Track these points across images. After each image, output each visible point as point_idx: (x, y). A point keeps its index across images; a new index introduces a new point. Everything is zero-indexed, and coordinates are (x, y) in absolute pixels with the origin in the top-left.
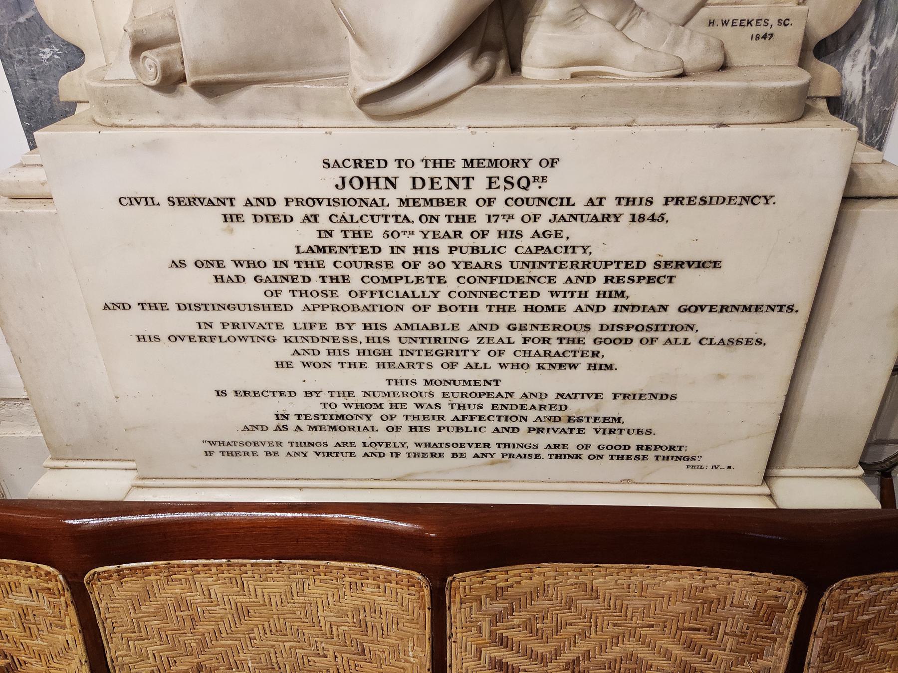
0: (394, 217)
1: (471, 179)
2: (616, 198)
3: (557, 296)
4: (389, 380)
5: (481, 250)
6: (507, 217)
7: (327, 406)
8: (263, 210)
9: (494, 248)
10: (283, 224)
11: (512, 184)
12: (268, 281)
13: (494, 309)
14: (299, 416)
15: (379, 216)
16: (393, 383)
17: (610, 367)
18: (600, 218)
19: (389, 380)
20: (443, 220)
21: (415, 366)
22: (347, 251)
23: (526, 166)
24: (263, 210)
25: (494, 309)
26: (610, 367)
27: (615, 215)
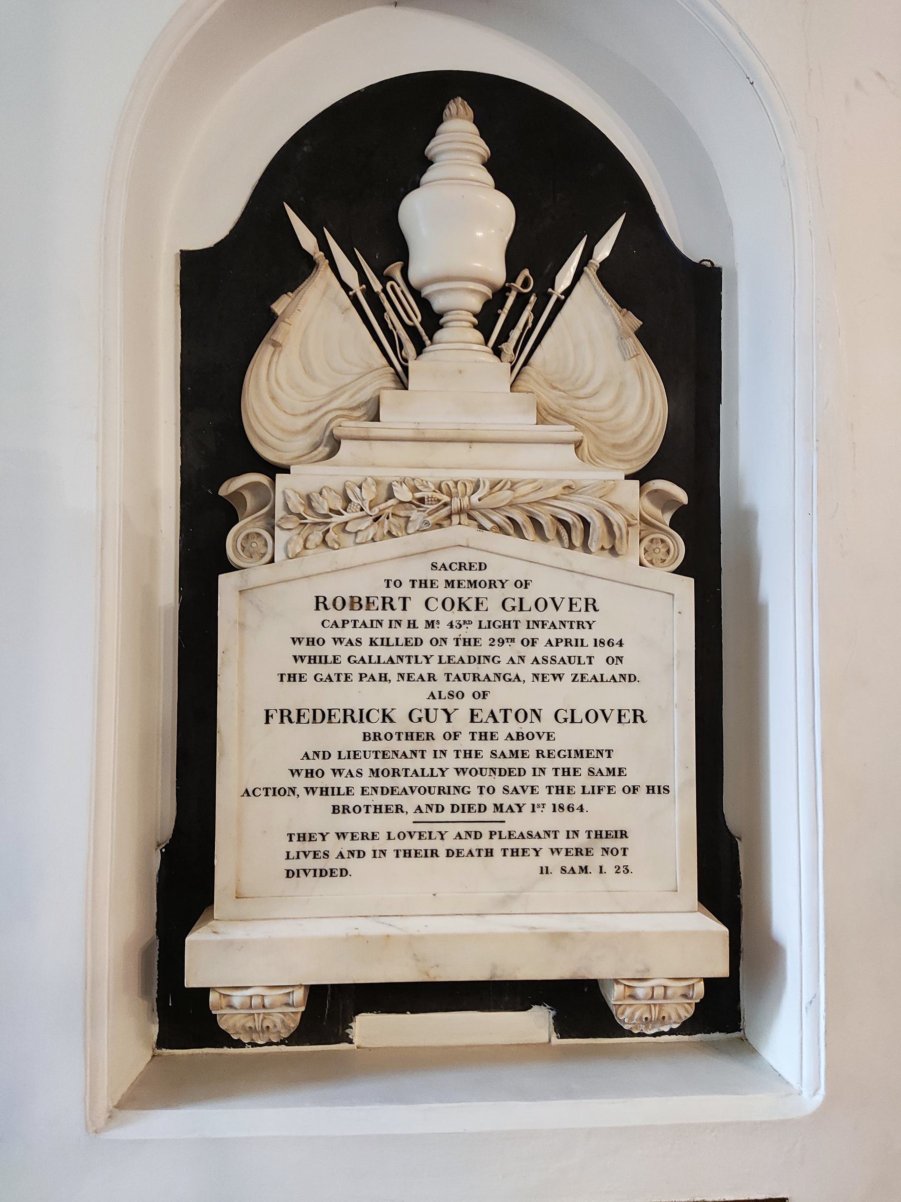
9: (489, 622)
11: (453, 696)
17: (631, 678)
26: (631, 678)
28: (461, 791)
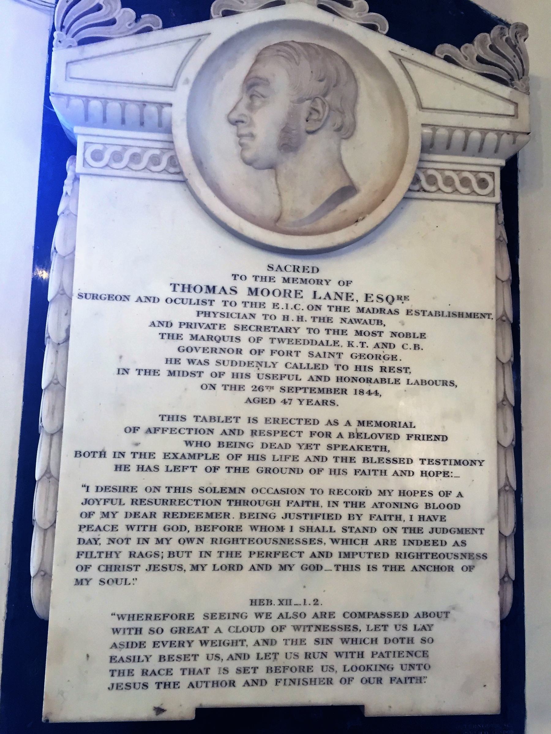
0: (192, 468)
1: (238, 419)
2: (110, 671)
3: (261, 617)
4: (175, 285)
5: (412, 335)
6: (269, 388)
7: (228, 304)
8: (146, 462)
10: (268, 405)
12: (379, 519)
13: (166, 337)
14: (423, 460)
15: (183, 552)
16: (179, 288)
18: (148, 515)
19: (175, 285)
20: (323, 333)
21: (293, 354)
22: (476, 532)
23: (296, 332)
24: (146, 462)
25: (166, 337)
27: (116, 552)
28: (414, 655)
